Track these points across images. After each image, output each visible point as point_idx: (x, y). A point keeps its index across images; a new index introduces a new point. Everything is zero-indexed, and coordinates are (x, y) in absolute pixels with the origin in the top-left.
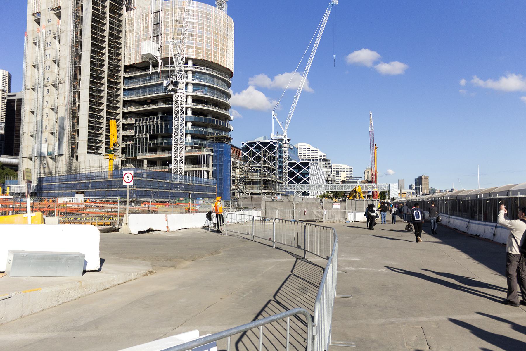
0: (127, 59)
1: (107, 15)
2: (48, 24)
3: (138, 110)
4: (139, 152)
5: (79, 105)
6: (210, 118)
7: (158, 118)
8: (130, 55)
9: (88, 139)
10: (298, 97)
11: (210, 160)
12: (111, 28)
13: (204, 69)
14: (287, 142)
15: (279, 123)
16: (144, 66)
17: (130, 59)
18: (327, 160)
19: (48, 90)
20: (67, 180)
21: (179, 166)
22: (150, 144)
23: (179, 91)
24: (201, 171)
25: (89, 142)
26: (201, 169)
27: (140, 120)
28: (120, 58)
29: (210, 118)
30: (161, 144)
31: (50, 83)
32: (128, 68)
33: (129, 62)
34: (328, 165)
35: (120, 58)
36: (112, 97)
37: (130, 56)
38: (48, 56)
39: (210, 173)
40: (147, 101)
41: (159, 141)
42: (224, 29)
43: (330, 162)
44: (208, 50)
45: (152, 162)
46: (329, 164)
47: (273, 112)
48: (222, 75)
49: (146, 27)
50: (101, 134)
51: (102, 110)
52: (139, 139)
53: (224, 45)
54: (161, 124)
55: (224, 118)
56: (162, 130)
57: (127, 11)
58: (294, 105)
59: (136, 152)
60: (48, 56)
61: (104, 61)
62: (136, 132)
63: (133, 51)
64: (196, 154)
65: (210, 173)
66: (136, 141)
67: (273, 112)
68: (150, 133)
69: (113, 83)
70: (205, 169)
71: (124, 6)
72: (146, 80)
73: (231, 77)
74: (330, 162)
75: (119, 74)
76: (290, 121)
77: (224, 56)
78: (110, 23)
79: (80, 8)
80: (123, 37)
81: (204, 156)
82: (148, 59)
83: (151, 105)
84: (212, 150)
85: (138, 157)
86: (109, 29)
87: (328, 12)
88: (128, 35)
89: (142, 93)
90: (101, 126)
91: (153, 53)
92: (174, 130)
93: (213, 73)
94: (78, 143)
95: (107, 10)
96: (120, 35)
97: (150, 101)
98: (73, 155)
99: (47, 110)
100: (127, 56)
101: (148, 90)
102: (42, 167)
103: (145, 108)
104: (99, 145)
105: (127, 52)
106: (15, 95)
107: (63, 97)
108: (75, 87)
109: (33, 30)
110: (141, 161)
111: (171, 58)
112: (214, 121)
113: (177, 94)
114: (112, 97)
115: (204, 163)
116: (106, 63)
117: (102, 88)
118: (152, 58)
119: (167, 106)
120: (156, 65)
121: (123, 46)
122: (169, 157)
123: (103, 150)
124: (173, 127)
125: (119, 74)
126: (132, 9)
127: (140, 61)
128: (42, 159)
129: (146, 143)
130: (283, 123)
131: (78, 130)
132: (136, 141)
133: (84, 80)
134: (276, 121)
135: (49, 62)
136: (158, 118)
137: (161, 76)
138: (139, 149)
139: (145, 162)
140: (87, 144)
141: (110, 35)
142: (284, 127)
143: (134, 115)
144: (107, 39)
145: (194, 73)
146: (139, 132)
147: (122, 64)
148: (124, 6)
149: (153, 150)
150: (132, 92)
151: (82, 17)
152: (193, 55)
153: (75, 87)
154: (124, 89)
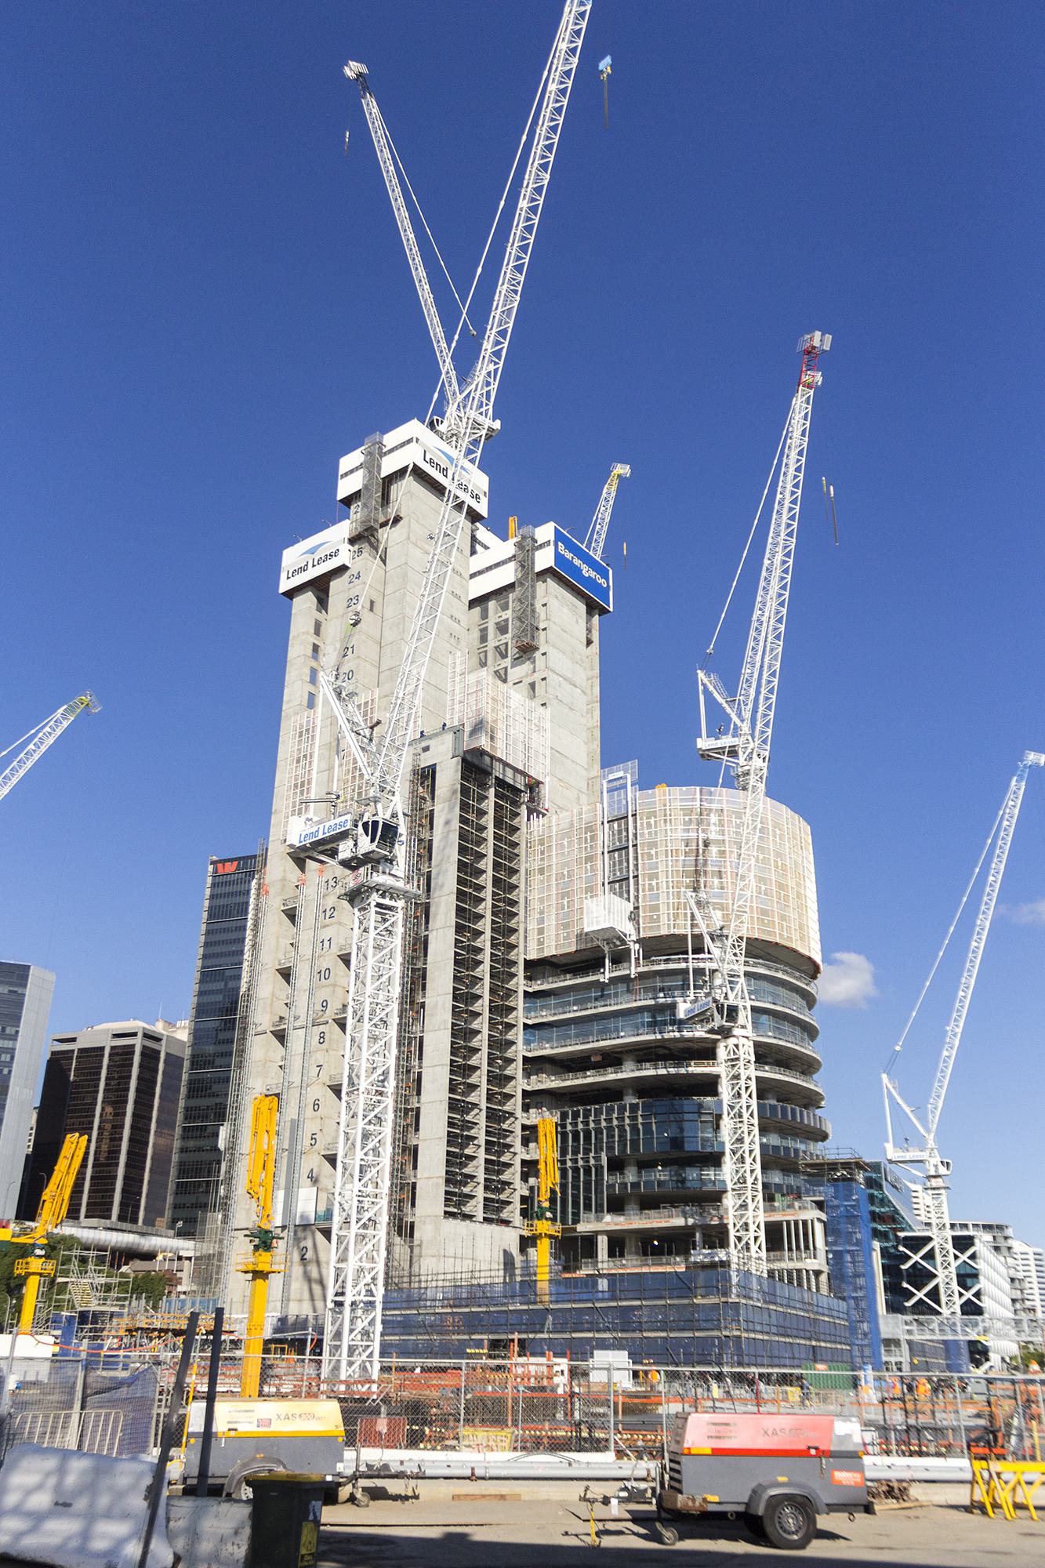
1: (490, 833)
5: (420, 1074)
6: (773, 1102)
7: (622, 1109)
8: (541, 931)
9: (447, 1172)
10: (959, 1030)
14: (943, 1170)
15: (907, 1110)
16: (586, 959)
17: (540, 943)
18: (1000, 1227)
21: (747, 1258)
23: (736, 1031)
24: (799, 1271)
25: (448, 1181)
26: (799, 1265)
28: (512, 939)
32: (535, 968)
34: (1001, 1243)
35: (512, 939)
37: (542, 933)
38: (326, 944)
39: (823, 1278)
40: (589, 1057)
41: (631, 1176)
43: (1009, 1232)
44: (764, 912)
49: (590, 859)
50: (509, 1165)
55: (806, 1101)
58: (949, 1053)
60: (326, 944)
61: (480, 950)
63: (551, 922)
65: (823, 1278)
67: (884, 1076)
68: (610, 1148)
71: (524, 807)
72: (589, 1000)
74: (1009, 1232)
75: (511, 985)
76: (941, 1104)
78: (495, 853)
80: (522, 886)
81: (805, 1223)
83: (610, 1070)
85: (582, 1228)
86: (494, 869)
89: (577, 1036)
91: (618, 928)
93: (780, 975)
95: (489, 820)
96: (513, 880)
97: (599, 1058)
98: (403, 1228)
100: (533, 937)
102: (296, 1257)
103: (591, 1078)
104: (503, 1197)
105: (533, 926)
106: (74, 1040)
109: (284, 879)
110: (590, 1241)
112: (784, 1110)
113: (732, 1041)
114: (499, 1045)
115: (807, 1248)
117: (475, 1025)
118: (614, 938)
119: (662, 1072)
120: (620, 958)
121: (520, 909)
122: (686, 1226)
123: (476, 1207)
125: (511, 985)
130: (921, 1111)
131: (416, 1148)
134: (894, 1104)
136: (622, 1109)
139: (603, 1243)
140: (443, 1188)
141: (496, 882)
143: (548, 1099)
144: (488, 893)
145: (747, 974)
146: (576, 1152)
147: (520, 956)
148: (524, 807)
149: (617, 1206)
150: (545, 1033)
151: (431, 841)
154: (526, 1026)
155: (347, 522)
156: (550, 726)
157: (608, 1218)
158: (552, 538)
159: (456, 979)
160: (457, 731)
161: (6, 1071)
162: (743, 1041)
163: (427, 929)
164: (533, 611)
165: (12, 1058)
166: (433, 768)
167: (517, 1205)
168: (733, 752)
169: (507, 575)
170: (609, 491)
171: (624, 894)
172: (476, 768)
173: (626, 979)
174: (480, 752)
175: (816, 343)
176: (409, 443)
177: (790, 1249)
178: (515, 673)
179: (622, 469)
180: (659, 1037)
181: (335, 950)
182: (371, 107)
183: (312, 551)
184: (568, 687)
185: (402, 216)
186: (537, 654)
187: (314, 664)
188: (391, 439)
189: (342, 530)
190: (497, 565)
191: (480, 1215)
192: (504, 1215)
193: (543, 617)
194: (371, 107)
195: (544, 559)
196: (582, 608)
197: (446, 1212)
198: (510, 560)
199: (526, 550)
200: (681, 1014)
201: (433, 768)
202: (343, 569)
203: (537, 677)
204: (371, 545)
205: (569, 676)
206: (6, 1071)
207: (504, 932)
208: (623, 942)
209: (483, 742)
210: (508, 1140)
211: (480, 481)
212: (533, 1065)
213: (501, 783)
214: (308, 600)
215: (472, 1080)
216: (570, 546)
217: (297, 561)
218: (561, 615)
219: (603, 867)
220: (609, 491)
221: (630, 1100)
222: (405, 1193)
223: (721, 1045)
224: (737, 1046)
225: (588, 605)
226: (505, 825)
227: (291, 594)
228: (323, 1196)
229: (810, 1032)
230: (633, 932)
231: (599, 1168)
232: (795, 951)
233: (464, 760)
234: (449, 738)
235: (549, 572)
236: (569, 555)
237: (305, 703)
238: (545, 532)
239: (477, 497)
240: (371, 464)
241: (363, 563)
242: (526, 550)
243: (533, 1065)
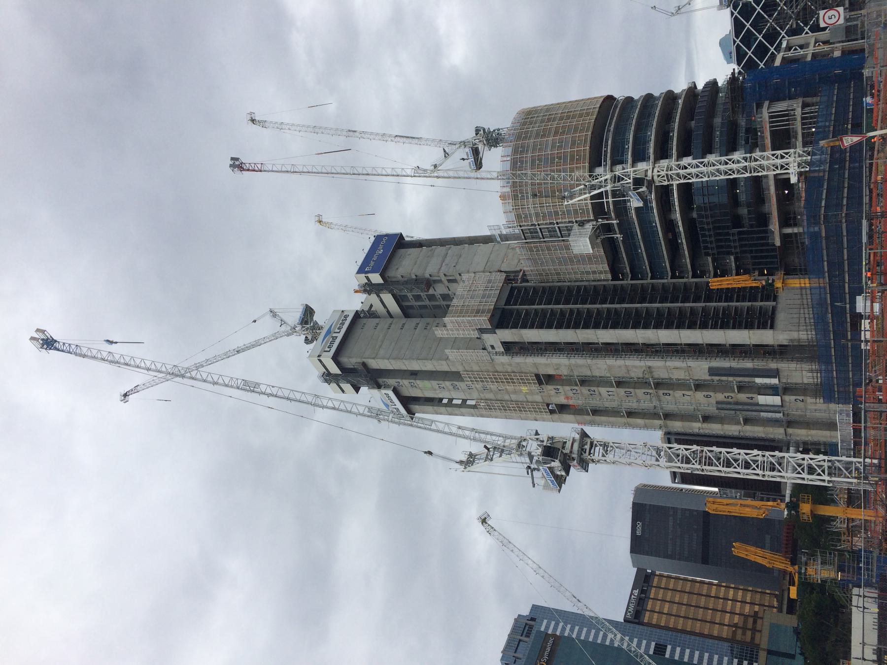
2: (563, 393)
4: (768, 244)
5: (685, 344)
8: (594, 272)
11: (781, 106)
13: (606, 146)
16: (610, 248)
17: (601, 272)
20: (828, 363)
22: (751, 226)
23: (649, 178)
24: (803, 119)
26: (799, 119)
32: (615, 271)
33: (606, 272)
36: (666, 294)
40: (670, 240)
41: (743, 211)
42: (535, 123)
45: (787, 220)
52: (741, 246)
57: (527, 281)
59: (767, 251)
62: (729, 253)
64: (768, 134)
65: (809, 100)
66: (745, 252)
68: (728, 228)
69: (642, 295)
70: (798, 112)
77: (581, 116)
81: (771, 117)
82: (599, 241)
84: (759, 106)
85: (778, 243)
92: (722, 177)
97: (670, 234)
107: (674, 371)
108: (657, 351)
110: (785, 237)
111: (592, 198)
114: (666, 294)
124: (717, 178)
132: (745, 252)
138: (763, 245)
139: (789, 231)
145: (614, 163)
152: (584, 167)
153: (657, 351)
157: (771, 227)
158: (364, 275)
161: (695, 513)
162: (655, 170)
163: (598, 344)
171: (569, 230)
172: (502, 319)
184: (448, 258)
191: (771, 304)
197: (772, 327)
198: (378, 296)
200: (641, 204)
203: (444, 279)
208: (598, 227)
212: (676, 268)
213: (508, 302)
221: (695, 215)
223: (657, 184)
224: (659, 176)
225: (399, 248)
230: (591, 224)
231: (740, 233)
233: (497, 328)
234: (485, 336)
235: (382, 276)
236: (372, 263)
243: (676, 268)
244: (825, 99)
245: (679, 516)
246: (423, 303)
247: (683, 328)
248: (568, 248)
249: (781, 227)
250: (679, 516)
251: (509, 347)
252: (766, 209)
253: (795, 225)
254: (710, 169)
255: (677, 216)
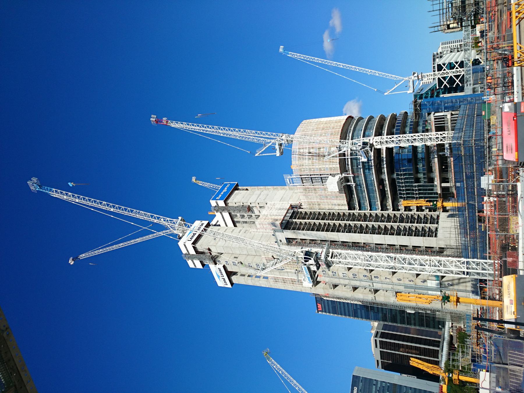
0: (343, 208)
3: (390, 196)
5: (388, 245)
6: (395, 130)
7: (398, 179)
8: (339, 205)
12: (318, 219)
14: (416, 75)
15: (396, 86)
16: (347, 190)
17: (343, 205)
18: (434, 56)
19: (375, 277)
22: (425, 182)
23: (371, 142)
24: (451, 121)
25: (424, 236)
26: (449, 121)
27: (401, 194)
28: (342, 214)
29: (395, 130)
30: (424, 174)
31: (368, 274)
32: (351, 207)
34: (439, 56)
36: (377, 219)
37: (340, 204)
38: (344, 275)
39: (453, 113)
41: (421, 176)
43: (435, 53)
46: (437, 54)
47: (385, 94)
48: (353, 123)
49: (315, 189)
51: (392, 227)
53: (325, 123)
54: (404, 170)
55: (394, 120)
56: (410, 174)
58: (377, 73)
60: (344, 275)
61: (345, 224)
63: (335, 202)
65: (453, 113)
67: (385, 94)
68: (412, 182)
70: (449, 117)
71: (299, 210)
72: (361, 190)
73: (353, 118)
74: (435, 53)
75: (357, 215)
78: (313, 219)
79: (304, 241)
80: (324, 211)
81: (435, 119)
83: (385, 183)
85: (439, 192)
87: (290, 54)
88: (322, 206)
90: (407, 228)
93: (352, 129)
94: (426, 247)
96: (322, 213)
97: (381, 186)
98: (441, 251)
99: (394, 279)
100: (340, 208)
101: (370, 187)
102: (451, 287)
103: (388, 189)
105: (337, 207)
106: (378, 361)
109: (323, 288)
110: (443, 189)
112: (397, 126)
113: (374, 144)
114: (377, 219)
115: (443, 118)
116: (348, 223)
117: (371, 226)
119: (385, 166)
120: (347, 180)
121: (332, 211)
123: (433, 226)
125: (357, 215)
126: (301, 205)
127: (344, 195)
128: (443, 286)
129: (423, 186)
130: (396, 83)
131: (413, 246)
133: (364, 239)
135: (350, 274)
136: (398, 179)
137: (356, 174)
139: (444, 185)
140: (427, 238)
142: (400, 81)
143: (395, 203)
144: (327, 222)
147: (347, 212)
148: (299, 210)
149: (432, 180)
150: (373, 204)
155: (210, 265)
156: (273, 202)
157: (436, 183)
159: (355, 232)
160: (275, 231)
161: (388, 384)
164: (237, 207)
165: (384, 382)
166: (287, 239)
167: (432, 213)
168: (281, 145)
169: (226, 215)
170: (200, 183)
172: (286, 225)
173: (354, 178)
174: (281, 224)
175: (154, 120)
176: (185, 245)
177: (444, 124)
178: (257, 213)
179: (194, 179)
180: (373, 167)
181: (347, 272)
182: (83, 256)
183: (219, 277)
184: (261, 196)
185: (115, 247)
186: (251, 206)
187: (254, 277)
188: (184, 251)
189: (212, 267)
190: (223, 218)
192: (434, 230)
193: (239, 204)
194: (83, 256)
195: (221, 203)
196: (236, 191)
199: (218, 209)
201: (287, 239)
202: (224, 267)
203: (258, 206)
204: (217, 258)
205: (257, 196)
206: (388, 384)
207: (339, 217)
209: (278, 223)
210: (407, 228)
211: (197, 223)
213: (291, 217)
214: (234, 278)
215: (389, 227)
216: (218, 195)
217: (222, 282)
218: (238, 198)
219: (318, 185)
220: (200, 183)
221: (395, 176)
222: (429, 251)
223: (376, 147)
226: (305, 216)
227: (232, 284)
228: (430, 278)
229: (371, 118)
231: (419, 186)
232: (344, 124)
233: (284, 229)
234: (277, 234)
235: (225, 202)
236: (220, 196)
237: (266, 280)
238: (213, 203)
239: (202, 224)
240: (192, 257)
241: (223, 260)
242: (218, 209)
243: (384, 207)
244: (461, 112)
245: (379, 385)
246: (245, 220)
247: (387, 234)
248: (325, 189)
249: (441, 183)
250: (379, 385)
251: (289, 241)
252: (432, 175)
253: (448, 182)
254: (405, 141)
255: (385, 177)
